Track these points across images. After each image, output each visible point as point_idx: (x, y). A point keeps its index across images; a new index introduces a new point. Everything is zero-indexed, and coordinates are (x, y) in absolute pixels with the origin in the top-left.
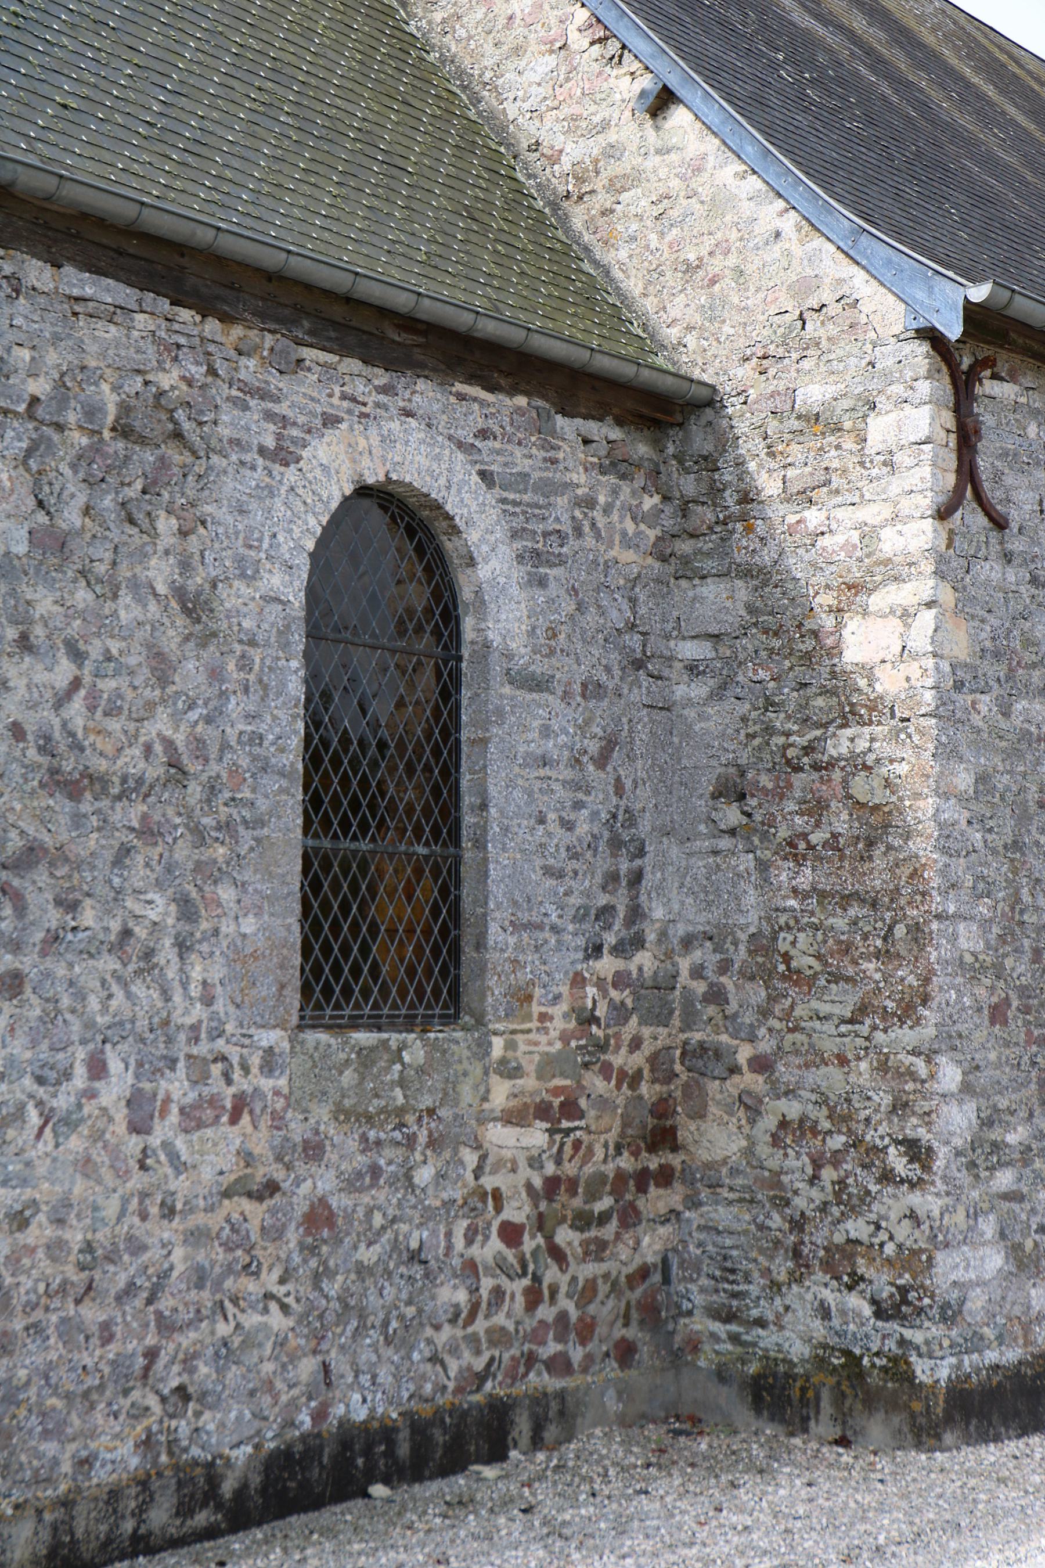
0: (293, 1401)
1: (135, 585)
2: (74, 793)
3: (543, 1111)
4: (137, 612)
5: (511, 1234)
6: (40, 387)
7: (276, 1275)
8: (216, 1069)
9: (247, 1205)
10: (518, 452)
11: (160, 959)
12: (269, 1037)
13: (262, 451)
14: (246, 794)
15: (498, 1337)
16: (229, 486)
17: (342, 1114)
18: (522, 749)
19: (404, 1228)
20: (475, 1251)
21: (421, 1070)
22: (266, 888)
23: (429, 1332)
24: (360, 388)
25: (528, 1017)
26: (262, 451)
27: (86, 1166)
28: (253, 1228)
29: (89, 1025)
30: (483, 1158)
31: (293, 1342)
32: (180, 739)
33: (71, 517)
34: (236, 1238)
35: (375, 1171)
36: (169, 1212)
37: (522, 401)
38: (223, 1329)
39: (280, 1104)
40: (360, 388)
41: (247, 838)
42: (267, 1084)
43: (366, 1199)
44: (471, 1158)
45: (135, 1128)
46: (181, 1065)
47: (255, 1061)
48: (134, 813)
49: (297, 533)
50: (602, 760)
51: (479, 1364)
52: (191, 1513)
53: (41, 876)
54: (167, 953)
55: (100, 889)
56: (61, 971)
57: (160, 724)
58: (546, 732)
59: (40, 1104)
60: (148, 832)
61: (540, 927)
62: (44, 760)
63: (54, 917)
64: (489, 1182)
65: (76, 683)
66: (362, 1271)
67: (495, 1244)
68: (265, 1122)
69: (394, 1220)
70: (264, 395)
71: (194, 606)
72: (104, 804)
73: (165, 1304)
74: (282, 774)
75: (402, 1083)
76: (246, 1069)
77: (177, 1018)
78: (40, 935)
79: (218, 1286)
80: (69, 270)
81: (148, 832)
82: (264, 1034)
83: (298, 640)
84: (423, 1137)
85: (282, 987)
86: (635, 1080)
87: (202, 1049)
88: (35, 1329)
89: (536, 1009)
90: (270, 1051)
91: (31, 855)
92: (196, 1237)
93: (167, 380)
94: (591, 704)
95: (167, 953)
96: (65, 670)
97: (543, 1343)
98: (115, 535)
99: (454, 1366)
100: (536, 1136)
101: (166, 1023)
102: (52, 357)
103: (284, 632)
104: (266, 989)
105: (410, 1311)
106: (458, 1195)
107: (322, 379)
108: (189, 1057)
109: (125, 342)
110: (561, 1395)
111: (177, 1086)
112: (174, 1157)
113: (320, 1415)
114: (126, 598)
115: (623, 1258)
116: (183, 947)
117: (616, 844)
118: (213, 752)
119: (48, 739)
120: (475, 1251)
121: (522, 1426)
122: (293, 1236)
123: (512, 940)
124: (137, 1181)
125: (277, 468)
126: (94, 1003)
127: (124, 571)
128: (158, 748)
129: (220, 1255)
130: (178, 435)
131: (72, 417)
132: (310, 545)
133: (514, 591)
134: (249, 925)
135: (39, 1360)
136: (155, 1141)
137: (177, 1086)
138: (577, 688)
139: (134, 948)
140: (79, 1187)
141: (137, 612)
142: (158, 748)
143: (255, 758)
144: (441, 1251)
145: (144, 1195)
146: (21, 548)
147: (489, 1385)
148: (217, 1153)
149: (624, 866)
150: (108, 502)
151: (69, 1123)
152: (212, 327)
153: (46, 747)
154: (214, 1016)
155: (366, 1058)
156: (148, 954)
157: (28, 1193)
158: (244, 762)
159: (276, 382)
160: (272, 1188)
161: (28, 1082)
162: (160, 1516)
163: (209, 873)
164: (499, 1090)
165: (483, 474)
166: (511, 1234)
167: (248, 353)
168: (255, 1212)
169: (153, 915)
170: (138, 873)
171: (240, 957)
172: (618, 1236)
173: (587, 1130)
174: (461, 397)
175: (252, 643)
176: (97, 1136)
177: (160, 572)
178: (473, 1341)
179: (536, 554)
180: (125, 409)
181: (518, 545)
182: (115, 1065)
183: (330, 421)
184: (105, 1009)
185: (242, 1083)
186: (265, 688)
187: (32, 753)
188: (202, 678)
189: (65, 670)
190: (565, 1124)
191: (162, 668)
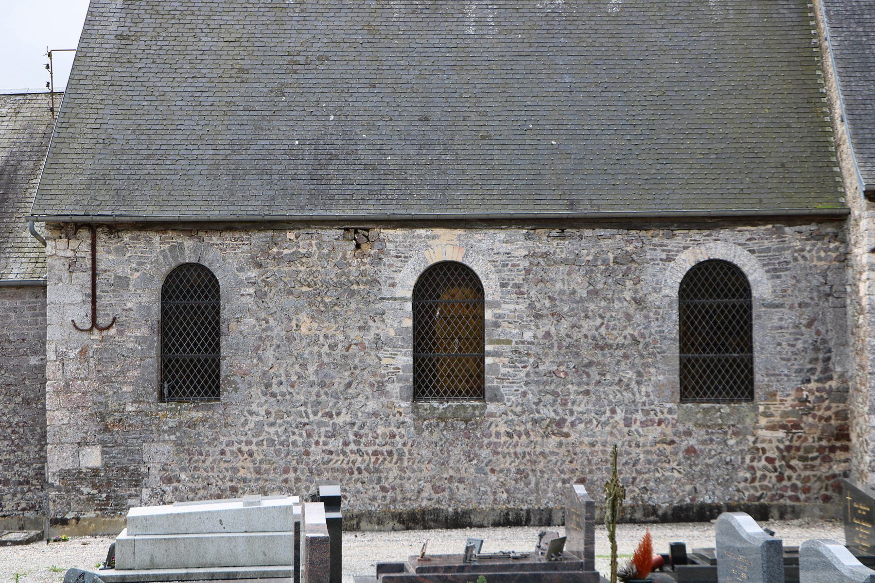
0: (684, 496)
1: (619, 299)
2: (602, 349)
3: (783, 427)
4: (620, 305)
5: (770, 460)
6: (590, 258)
7: (676, 463)
8: (652, 413)
9: (665, 446)
10: (766, 242)
11: (632, 386)
12: (669, 405)
13: (661, 260)
14: (659, 345)
15: (766, 488)
16: (650, 270)
17: (696, 425)
18: (770, 325)
19: (724, 455)
20: (755, 464)
21: (728, 414)
22: (667, 368)
23: (736, 483)
24: (697, 237)
25: (776, 400)
26: (661, 260)
27: (611, 433)
28: (668, 452)
29: (610, 402)
30: (757, 439)
31: (683, 480)
32: (636, 334)
33: (600, 286)
34: (661, 453)
35: (711, 440)
36: (638, 446)
37: (770, 226)
38: (657, 475)
39: (674, 422)
40: (697, 237)
41: (659, 356)
42: (669, 417)
43: (709, 447)
44: (751, 439)
45: (626, 426)
46: (640, 411)
47: (665, 411)
48: (621, 353)
49: (674, 278)
50: (809, 325)
51: (758, 494)
52: (648, 516)
53: (594, 368)
54: (633, 385)
55: (612, 370)
56: (601, 389)
57: (629, 330)
58: (781, 319)
59: (596, 419)
60: (626, 356)
61: (780, 375)
62: (594, 342)
63: (598, 378)
64: (759, 445)
65: (602, 324)
66: (707, 465)
67: (763, 462)
68: (670, 426)
69: (720, 453)
70: (661, 246)
71: (638, 302)
72: (612, 351)
73: (639, 467)
74: (671, 339)
75: (721, 417)
76: (662, 413)
77: (637, 400)
78: (594, 382)
79: (655, 464)
80: (597, 230)
81: (626, 356)
82: (669, 407)
83: (676, 306)
84: (730, 432)
85: (673, 393)
86: (828, 419)
87: (647, 407)
88: (599, 469)
89: (778, 398)
90: (670, 408)
91: (590, 364)
92: (647, 452)
93: (630, 248)
94: (803, 309)
95: (633, 385)
96: (599, 321)
97: (786, 491)
98: (613, 288)
99: (747, 494)
100: (781, 434)
101: (634, 401)
102: (593, 251)
103: (670, 305)
104: (668, 393)
105: (727, 477)
106: (746, 448)
107: (681, 237)
108: (642, 409)
109: (613, 242)
110: (793, 507)
111: (639, 416)
112: (638, 433)
113: (692, 500)
114: (616, 302)
115: (824, 470)
116: (639, 383)
117: (816, 349)
118: (647, 336)
119: (594, 337)
120: (755, 464)
121: (775, 513)
122: (681, 455)
123: (766, 379)
124: (627, 438)
125: (667, 263)
126: (611, 397)
127: (616, 296)
128: (628, 336)
129: (656, 457)
130: (633, 260)
131: (599, 263)
132: (680, 281)
133: (765, 281)
134: (661, 378)
135: (600, 476)
136: (633, 429)
137: (639, 416)
138: (796, 305)
139: (623, 385)
140: (609, 438)
141: (620, 305)
142: (628, 336)
143: (661, 336)
144: (739, 463)
145: (630, 442)
146: (585, 295)
147: (762, 501)
148: (654, 433)
149: (821, 356)
150: (610, 281)
151: (605, 424)
152: (643, 233)
153: (594, 338)
154: (650, 400)
155: (706, 411)
156: (628, 385)
157: (595, 439)
158: (658, 338)
159: (666, 241)
160: (672, 442)
161: (593, 414)
162: (638, 515)
163: (646, 365)
164: (764, 424)
165: (749, 251)
166: (770, 460)
167: (657, 237)
168: (669, 449)
169: (628, 376)
170: (623, 366)
171: (659, 387)
172: (821, 465)
173: (804, 433)
174: (739, 231)
175: (659, 308)
176: (614, 427)
177: (628, 295)
178: (755, 488)
179: (775, 270)
180: (615, 258)
181: (766, 268)
182: (618, 410)
183: (686, 248)
184: (615, 397)
185: (660, 416)
186: (664, 319)
187: (590, 341)
188: (642, 318)
189: (599, 321)
190: (794, 431)
191: (629, 317)
